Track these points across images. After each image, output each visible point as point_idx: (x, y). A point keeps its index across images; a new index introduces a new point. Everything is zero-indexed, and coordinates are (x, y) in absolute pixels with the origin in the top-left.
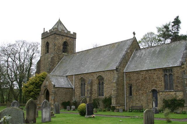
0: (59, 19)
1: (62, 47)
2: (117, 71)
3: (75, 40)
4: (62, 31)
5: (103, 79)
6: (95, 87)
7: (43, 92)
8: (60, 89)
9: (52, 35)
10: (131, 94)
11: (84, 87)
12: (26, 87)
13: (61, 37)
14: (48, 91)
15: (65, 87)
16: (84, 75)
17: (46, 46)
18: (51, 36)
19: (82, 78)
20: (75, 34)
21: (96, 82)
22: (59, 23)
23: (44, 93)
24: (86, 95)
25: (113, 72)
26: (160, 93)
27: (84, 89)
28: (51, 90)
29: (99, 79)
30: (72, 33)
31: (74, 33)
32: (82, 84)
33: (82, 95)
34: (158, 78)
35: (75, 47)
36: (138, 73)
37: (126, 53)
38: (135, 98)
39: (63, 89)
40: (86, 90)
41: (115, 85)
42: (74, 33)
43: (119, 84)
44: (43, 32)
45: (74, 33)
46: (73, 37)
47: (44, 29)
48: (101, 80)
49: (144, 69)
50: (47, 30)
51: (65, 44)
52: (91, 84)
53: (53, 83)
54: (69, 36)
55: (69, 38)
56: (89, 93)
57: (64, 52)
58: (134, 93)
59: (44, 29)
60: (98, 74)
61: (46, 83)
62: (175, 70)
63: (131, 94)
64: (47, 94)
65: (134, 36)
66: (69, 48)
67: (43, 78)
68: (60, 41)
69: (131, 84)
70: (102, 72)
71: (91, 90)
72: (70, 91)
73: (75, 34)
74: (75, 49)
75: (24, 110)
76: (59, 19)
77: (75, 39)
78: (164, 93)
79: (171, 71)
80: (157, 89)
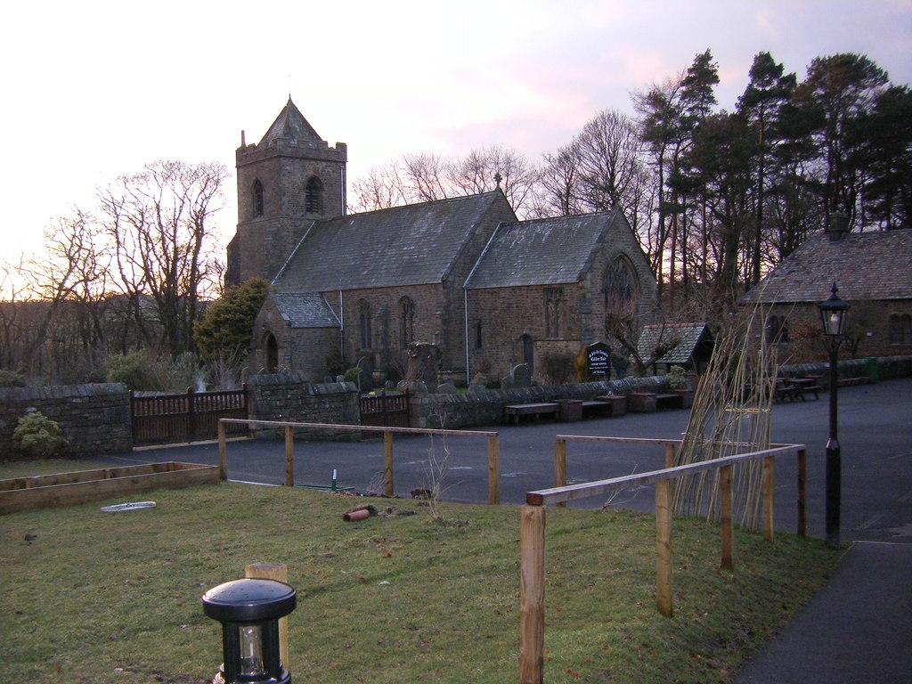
0: (290, 100)
1: (304, 194)
2: (444, 287)
3: (345, 169)
4: (302, 146)
5: (412, 305)
6: (395, 326)
7: (259, 340)
8: (306, 331)
9: (270, 159)
10: (479, 344)
11: (369, 323)
12: (207, 333)
13: (298, 164)
14: (272, 337)
15: (318, 324)
16: (368, 291)
17: (255, 195)
18: (267, 163)
19: (361, 299)
20: (342, 147)
21: (396, 312)
22: (291, 117)
23: (263, 342)
24: (373, 347)
25: (437, 289)
26: (539, 343)
27: (370, 329)
28: (282, 336)
29: (405, 305)
30: (332, 145)
31: (338, 144)
32: (363, 315)
33: (364, 347)
34: (536, 308)
35: (345, 183)
36: (493, 292)
37: (471, 239)
38: (488, 354)
39: (313, 330)
40: (373, 333)
41: (439, 321)
42: (338, 145)
43: (450, 322)
44: (239, 145)
45: (338, 144)
46: (339, 155)
47: (243, 132)
48: (408, 306)
49: (507, 285)
50: (254, 139)
51: (313, 185)
52: (386, 318)
53: (285, 317)
54: (323, 156)
55: (324, 164)
56: (379, 341)
57: (309, 210)
58: (486, 343)
59: (243, 132)
60: (403, 293)
61: (265, 315)
62: (567, 291)
63: (479, 344)
64: (272, 345)
65: (498, 185)
66: (324, 194)
67: (258, 300)
68: (295, 177)
69: (480, 321)
70: (410, 288)
71: (385, 333)
72: (333, 335)
73: (342, 147)
74: (345, 196)
75: (642, 641)
76: (290, 100)
77: (344, 163)
78: (545, 343)
79: (561, 292)
80: (533, 334)
